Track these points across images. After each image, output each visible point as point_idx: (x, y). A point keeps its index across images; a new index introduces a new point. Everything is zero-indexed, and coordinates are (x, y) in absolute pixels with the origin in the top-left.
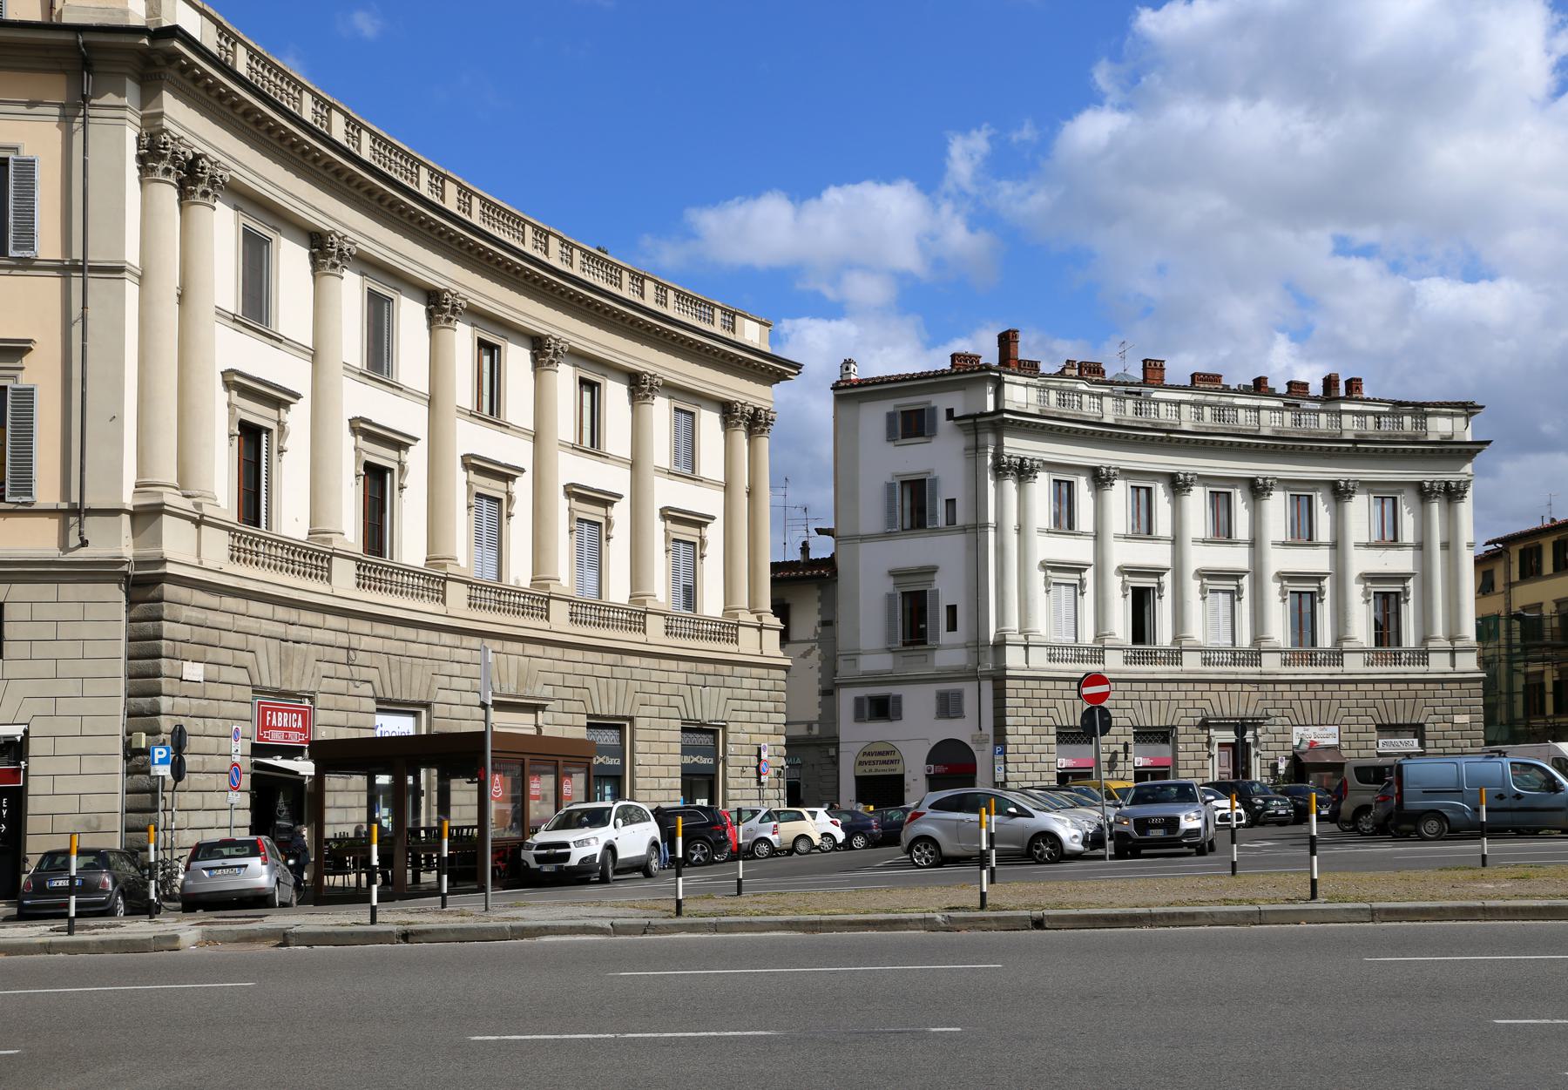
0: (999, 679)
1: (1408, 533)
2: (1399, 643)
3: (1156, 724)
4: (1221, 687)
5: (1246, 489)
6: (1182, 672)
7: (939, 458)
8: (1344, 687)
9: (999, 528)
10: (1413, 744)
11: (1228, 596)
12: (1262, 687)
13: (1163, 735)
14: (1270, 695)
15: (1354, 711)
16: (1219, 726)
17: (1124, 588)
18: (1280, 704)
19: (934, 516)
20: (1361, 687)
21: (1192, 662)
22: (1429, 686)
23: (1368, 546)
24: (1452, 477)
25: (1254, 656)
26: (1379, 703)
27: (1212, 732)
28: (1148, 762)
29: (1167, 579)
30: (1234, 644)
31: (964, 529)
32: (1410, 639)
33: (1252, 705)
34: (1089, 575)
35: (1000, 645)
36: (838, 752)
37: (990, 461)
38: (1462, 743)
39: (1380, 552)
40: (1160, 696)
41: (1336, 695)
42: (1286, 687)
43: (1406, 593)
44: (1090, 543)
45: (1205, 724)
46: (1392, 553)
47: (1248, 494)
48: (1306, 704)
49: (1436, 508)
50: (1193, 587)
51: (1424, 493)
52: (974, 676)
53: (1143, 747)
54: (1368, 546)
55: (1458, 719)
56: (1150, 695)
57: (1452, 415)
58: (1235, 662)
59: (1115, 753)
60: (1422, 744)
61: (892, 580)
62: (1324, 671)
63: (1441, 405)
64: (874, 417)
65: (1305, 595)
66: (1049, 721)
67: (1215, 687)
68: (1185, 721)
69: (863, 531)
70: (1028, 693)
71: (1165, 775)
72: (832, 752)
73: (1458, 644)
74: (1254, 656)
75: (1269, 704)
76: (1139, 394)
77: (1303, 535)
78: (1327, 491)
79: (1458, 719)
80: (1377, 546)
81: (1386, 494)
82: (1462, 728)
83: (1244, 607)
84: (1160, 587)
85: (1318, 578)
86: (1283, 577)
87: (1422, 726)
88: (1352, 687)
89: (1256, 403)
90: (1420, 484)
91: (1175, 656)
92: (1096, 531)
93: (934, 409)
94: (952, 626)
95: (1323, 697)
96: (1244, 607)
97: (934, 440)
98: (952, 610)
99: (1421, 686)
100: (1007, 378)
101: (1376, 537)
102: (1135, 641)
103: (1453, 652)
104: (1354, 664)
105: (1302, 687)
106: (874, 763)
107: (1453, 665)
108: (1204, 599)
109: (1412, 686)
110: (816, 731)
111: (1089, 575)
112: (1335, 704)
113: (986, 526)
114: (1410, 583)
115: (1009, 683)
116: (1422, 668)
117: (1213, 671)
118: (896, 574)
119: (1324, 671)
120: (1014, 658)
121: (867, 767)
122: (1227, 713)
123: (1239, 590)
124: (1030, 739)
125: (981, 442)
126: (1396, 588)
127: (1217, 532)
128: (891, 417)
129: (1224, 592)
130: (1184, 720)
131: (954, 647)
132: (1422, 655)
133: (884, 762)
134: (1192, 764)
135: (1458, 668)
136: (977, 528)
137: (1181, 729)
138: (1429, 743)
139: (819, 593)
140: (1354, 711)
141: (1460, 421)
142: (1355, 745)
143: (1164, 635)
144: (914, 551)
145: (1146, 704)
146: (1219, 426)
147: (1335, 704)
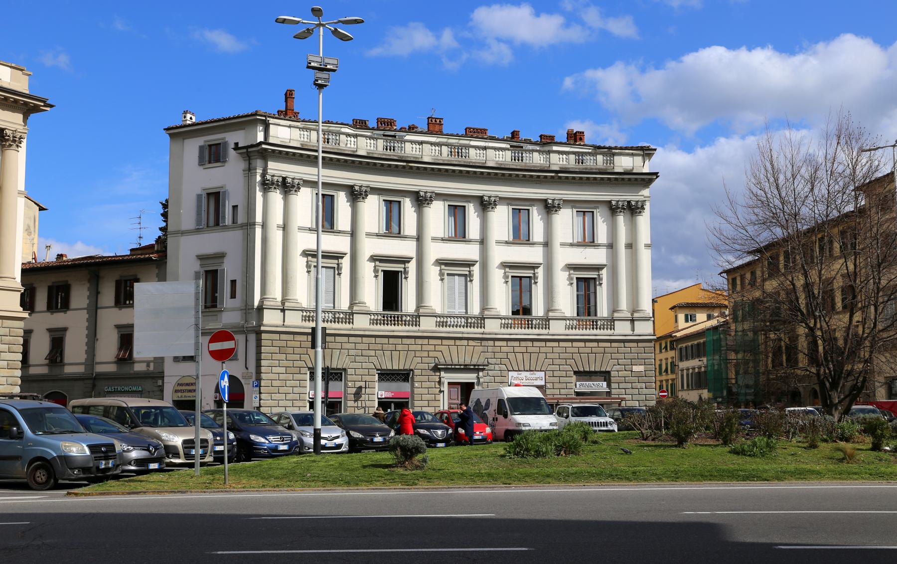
0: (259, 333)
1: (602, 236)
2: (596, 315)
3: (396, 367)
4: (452, 342)
5: (478, 204)
6: (419, 331)
7: (228, 176)
8: (549, 344)
9: (264, 226)
10: (603, 386)
11: (463, 279)
12: (484, 343)
13: (404, 376)
14: (490, 349)
15: (557, 361)
16: (447, 370)
17: (376, 271)
18: (498, 355)
19: (224, 217)
20: (562, 344)
21: (428, 325)
22: (614, 345)
23: (572, 245)
24: (633, 197)
25: (481, 320)
26: (576, 356)
27: (442, 374)
28: (389, 395)
29: (412, 267)
30: (466, 312)
31: (242, 226)
32: (603, 310)
33: (476, 356)
34: (476, 270)
35: (260, 309)
36: (163, 383)
37: (258, 178)
38: (639, 386)
39: (581, 249)
40: (399, 347)
41: (542, 350)
42: (504, 343)
43: (535, 277)
44: (413, 244)
45: (436, 369)
46: (590, 251)
47: (479, 208)
48: (519, 356)
49: (621, 219)
50: (432, 273)
51: (613, 209)
52: (243, 331)
53: (386, 384)
54: (572, 245)
55: (635, 368)
56: (391, 347)
57: (633, 155)
58: (467, 325)
59: (360, 388)
60: (609, 386)
61: (199, 262)
62: (533, 333)
63: (626, 148)
64: (192, 148)
65: (522, 279)
66: (302, 364)
67: (445, 342)
68: (420, 366)
69: (184, 227)
70: (283, 344)
71: (815, 391)
72: (160, 382)
73: (636, 315)
74: (481, 320)
75: (489, 355)
76: (395, 136)
77: (521, 236)
78: (541, 206)
79: (635, 368)
80: (578, 245)
81: (585, 209)
82: (639, 375)
83: (475, 287)
84: (406, 272)
85: (533, 267)
86: (505, 265)
87: (609, 372)
88: (556, 344)
89: (482, 144)
90: (609, 202)
91: (416, 319)
92: (284, 225)
93: (226, 144)
94: (233, 296)
95: (530, 353)
96: (475, 287)
97: (226, 164)
98: (233, 282)
99: (608, 344)
100: (271, 121)
101: (579, 238)
102: (385, 307)
103: (632, 321)
104: (557, 328)
105: (517, 344)
106: (183, 391)
107: (633, 330)
108: (442, 280)
109: (601, 344)
110: (151, 368)
111: (476, 270)
112: (542, 356)
113: (254, 224)
114: (604, 272)
115: (264, 336)
116: (609, 332)
117: (444, 331)
118: (201, 258)
119: (533, 333)
120: (271, 318)
121: (179, 394)
122: (455, 361)
123: (339, 267)
124: (282, 377)
125: (253, 165)
126: (529, 273)
127: (388, 227)
128: (201, 148)
129: (459, 275)
130: (418, 364)
131: (233, 310)
132: (611, 322)
133: (190, 391)
134: (425, 397)
135: (636, 332)
136: (250, 225)
137: (417, 372)
138: (613, 386)
139: (157, 271)
140: (557, 361)
141: (639, 159)
142: (556, 386)
143: (409, 303)
144: (211, 243)
145: (388, 353)
146: (455, 159)
147: (542, 356)
